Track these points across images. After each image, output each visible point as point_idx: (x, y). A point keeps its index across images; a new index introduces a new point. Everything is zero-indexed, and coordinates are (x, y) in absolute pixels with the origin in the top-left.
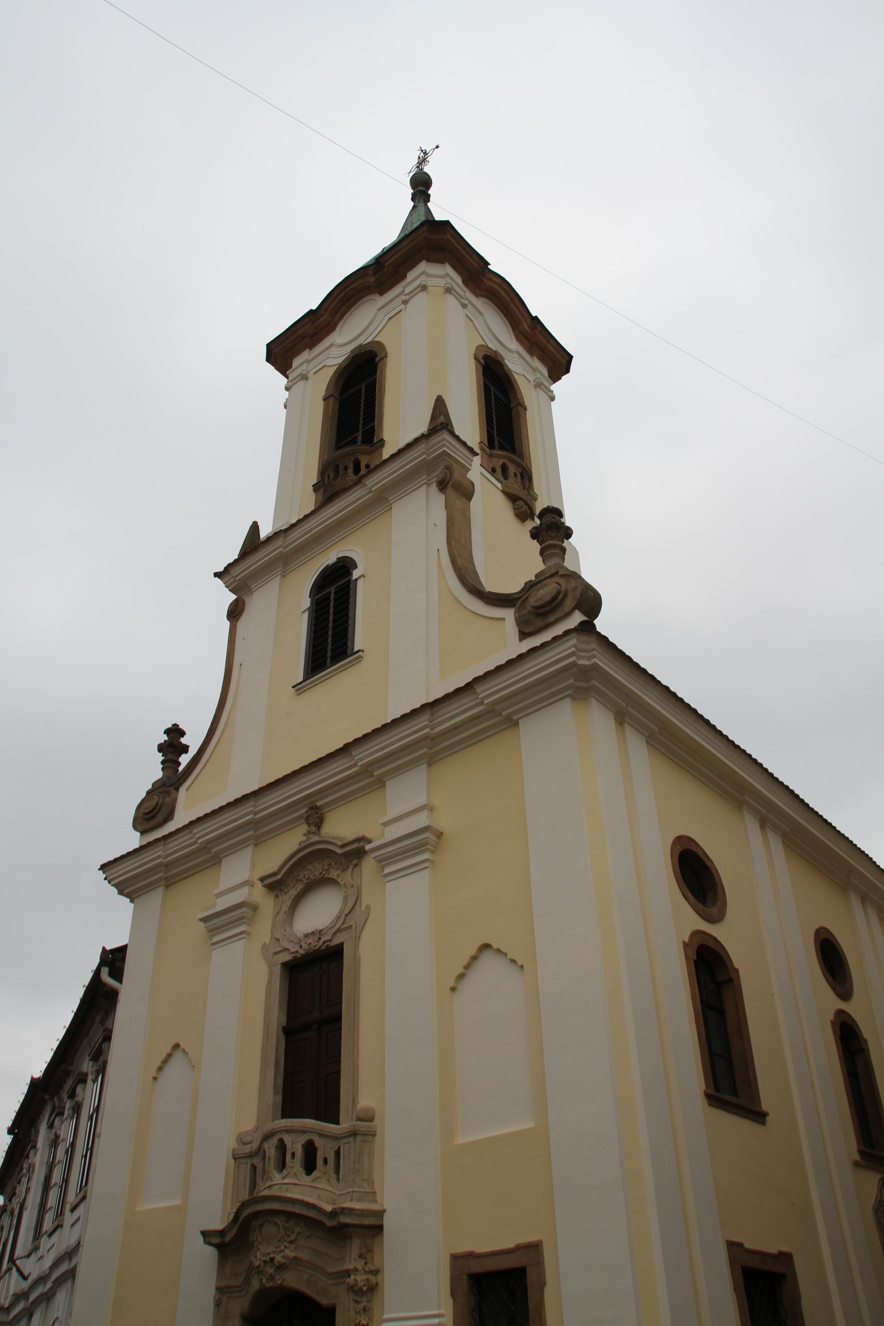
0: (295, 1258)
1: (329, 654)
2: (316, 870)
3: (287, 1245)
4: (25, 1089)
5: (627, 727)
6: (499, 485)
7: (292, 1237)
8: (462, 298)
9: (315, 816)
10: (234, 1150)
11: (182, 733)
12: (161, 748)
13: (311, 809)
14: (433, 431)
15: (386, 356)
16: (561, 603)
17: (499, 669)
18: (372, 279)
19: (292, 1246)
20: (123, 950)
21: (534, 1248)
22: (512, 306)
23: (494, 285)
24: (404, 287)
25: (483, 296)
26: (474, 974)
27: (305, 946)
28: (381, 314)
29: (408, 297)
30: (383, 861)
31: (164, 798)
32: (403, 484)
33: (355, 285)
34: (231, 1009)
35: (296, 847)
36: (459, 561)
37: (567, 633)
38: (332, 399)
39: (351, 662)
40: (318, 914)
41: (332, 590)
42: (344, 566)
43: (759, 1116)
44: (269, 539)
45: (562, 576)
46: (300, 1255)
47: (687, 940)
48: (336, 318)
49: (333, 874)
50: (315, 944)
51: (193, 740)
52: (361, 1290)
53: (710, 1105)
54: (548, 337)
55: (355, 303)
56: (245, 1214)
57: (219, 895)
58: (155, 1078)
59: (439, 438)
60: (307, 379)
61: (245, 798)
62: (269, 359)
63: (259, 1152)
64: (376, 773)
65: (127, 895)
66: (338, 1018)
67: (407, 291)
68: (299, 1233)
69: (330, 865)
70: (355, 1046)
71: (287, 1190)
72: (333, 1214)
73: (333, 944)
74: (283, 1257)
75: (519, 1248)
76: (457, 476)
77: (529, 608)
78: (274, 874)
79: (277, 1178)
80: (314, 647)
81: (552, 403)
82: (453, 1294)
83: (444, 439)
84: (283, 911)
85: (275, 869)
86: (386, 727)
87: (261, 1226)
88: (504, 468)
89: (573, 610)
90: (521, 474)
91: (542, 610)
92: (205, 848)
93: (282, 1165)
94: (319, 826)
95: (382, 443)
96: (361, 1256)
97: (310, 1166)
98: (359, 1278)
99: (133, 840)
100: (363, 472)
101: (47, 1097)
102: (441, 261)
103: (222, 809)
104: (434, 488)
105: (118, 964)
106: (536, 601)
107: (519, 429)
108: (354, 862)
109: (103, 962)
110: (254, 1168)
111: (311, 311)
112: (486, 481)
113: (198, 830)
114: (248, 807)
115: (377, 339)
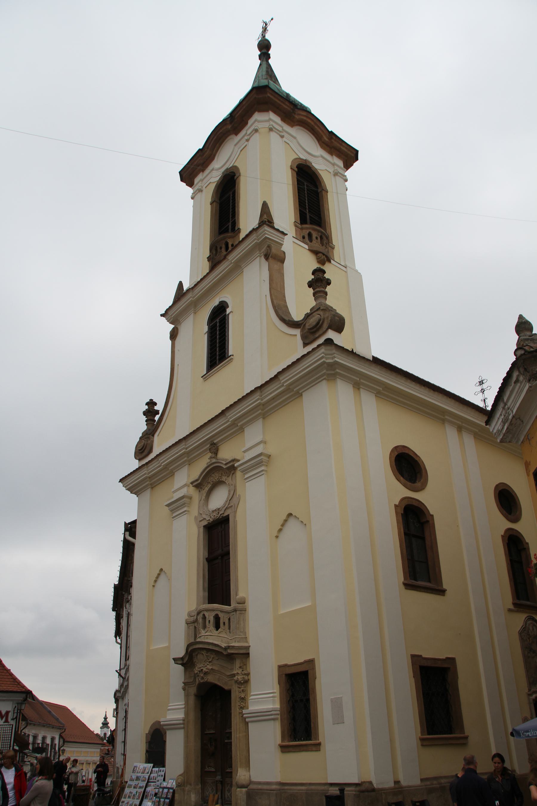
0: (212, 669)
2: (215, 477)
3: (208, 663)
6: (306, 247)
7: (210, 660)
8: (280, 132)
9: (214, 448)
10: (186, 620)
11: (155, 404)
12: (145, 413)
13: (211, 444)
14: (262, 223)
16: (321, 326)
18: (229, 127)
20: (134, 522)
21: (311, 662)
22: (316, 127)
24: (247, 131)
25: (297, 125)
26: (286, 529)
27: (212, 517)
29: (248, 137)
30: (245, 471)
31: (147, 441)
32: (247, 257)
33: (221, 131)
34: (181, 549)
35: (205, 466)
36: (275, 302)
37: (319, 346)
38: (214, 204)
39: (228, 362)
40: (218, 500)
41: (218, 321)
43: (442, 592)
44: (188, 290)
45: (322, 310)
46: (214, 668)
47: (397, 504)
50: (216, 516)
51: (160, 407)
52: (240, 682)
55: (223, 142)
56: (190, 650)
59: (261, 231)
61: (180, 441)
62: (182, 180)
63: (196, 621)
64: (239, 425)
65: (135, 493)
66: (228, 553)
68: (213, 658)
69: (222, 474)
70: (236, 568)
71: (207, 638)
72: (226, 649)
73: (225, 515)
75: (306, 662)
76: (274, 251)
77: (306, 330)
78: (197, 480)
79: (203, 632)
80: (211, 354)
81: (346, 183)
83: (265, 230)
84: (202, 499)
85: (197, 478)
87: (197, 655)
88: (310, 235)
90: (321, 238)
92: (166, 467)
93: (204, 627)
94: (216, 453)
95: (239, 230)
96: (240, 667)
97: (217, 627)
99: (135, 464)
100: (230, 249)
101: (124, 593)
102: (267, 110)
104: (263, 259)
105: (133, 530)
106: (309, 326)
107: (323, 205)
108: (232, 472)
110: (195, 627)
111: (200, 150)
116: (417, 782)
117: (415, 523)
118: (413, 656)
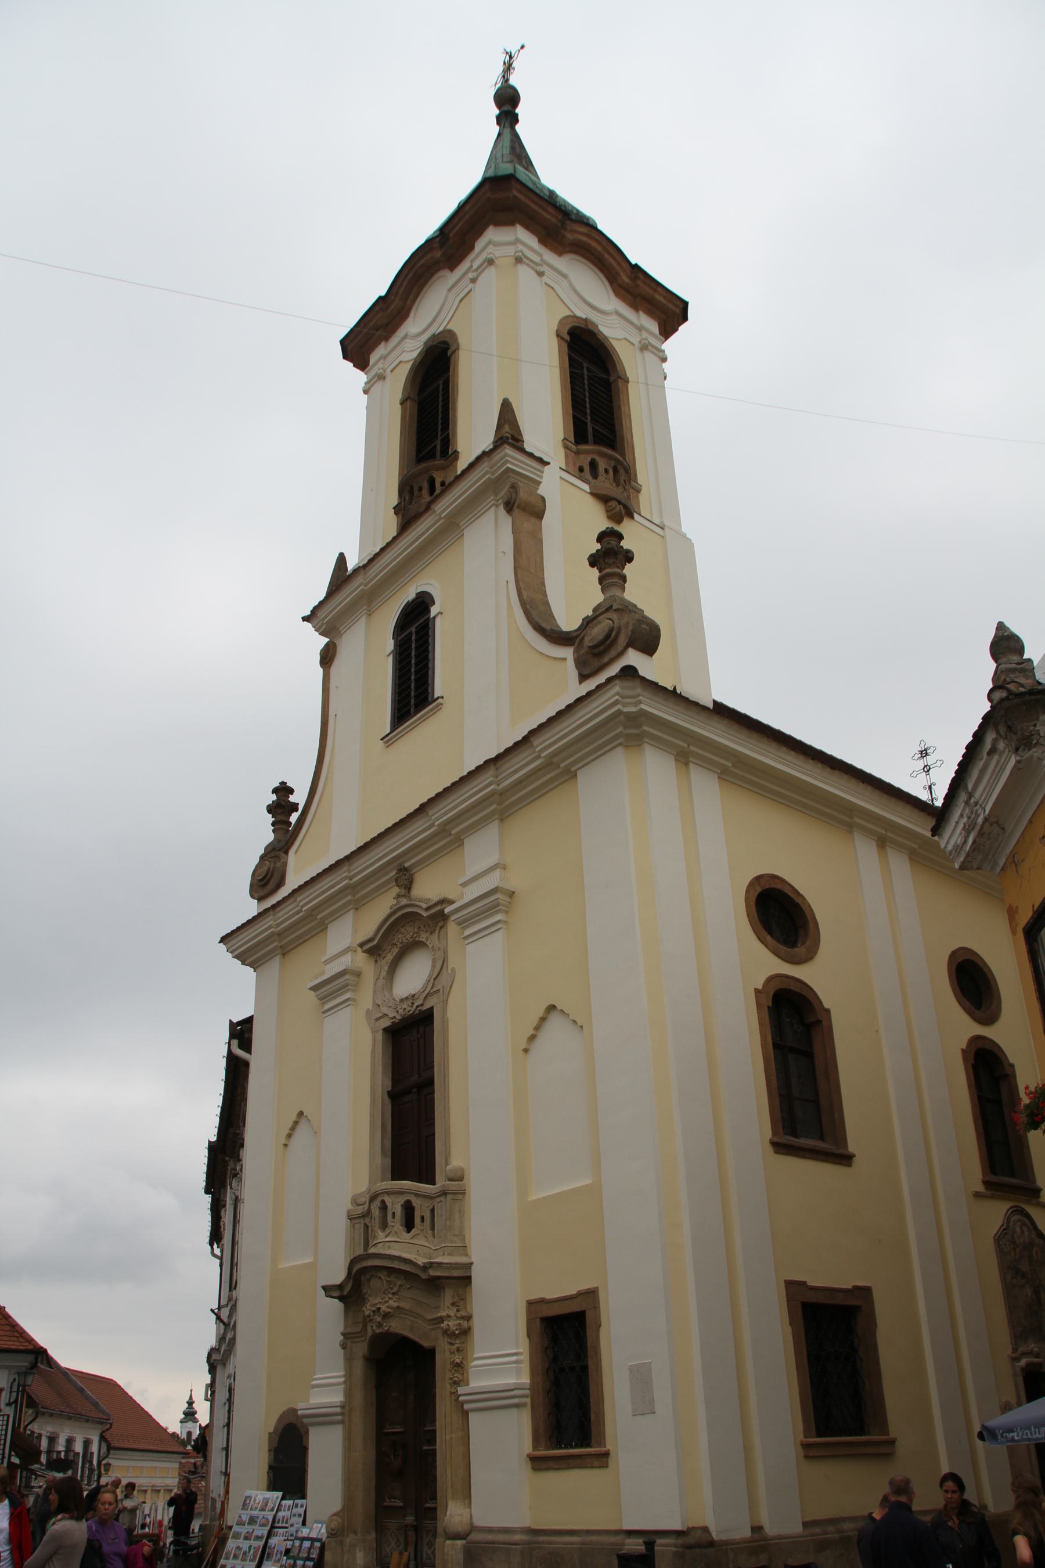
0: (398, 1307)
1: (412, 702)
2: (406, 934)
3: (391, 1296)
5: (692, 766)
7: (395, 1290)
9: (405, 878)
10: (349, 1211)
12: (270, 809)
13: (400, 870)
14: (500, 442)
17: (551, 721)
18: (438, 254)
19: (395, 1298)
20: (249, 1021)
21: (591, 1294)
24: (472, 262)
25: (569, 252)
28: (452, 295)
29: (475, 274)
30: (463, 923)
32: (471, 507)
34: (340, 1073)
35: (388, 911)
37: (609, 680)
38: (409, 402)
40: (413, 978)
41: (413, 629)
43: (845, 1159)
44: (356, 571)
46: (402, 1304)
48: (409, 302)
49: (423, 937)
50: (408, 1009)
51: (299, 797)
53: (776, 1152)
54: (654, 286)
57: (327, 962)
58: (286, 1145)
59: (502, 454)
60: (384, 378)
61: (338, 864)
63: (368, 1213)
65: (250, 965)
66: (431, 1082)
68: (401, 1286)
70: (446, 1109)
71: (389, 1247)
72: (425, 1268)
73: (424, 1008)
75: (581, 1294)
76: (523, 495)
78: (371, 940)
79: (381, 1236)
82: (529, 1336)
83: (506, 455)
85: (370, 935)
86: (463, 780)
87: (369, 1280)
88: (593, 465)
90: (615, 470)
91: (601, 648)
93: (384, 1226)
94: (408, 887)
95: (456, 454)
96: (453, 1304)
97: (409, 1225)
98: (451, 1324)
99: (251, 908)
102: (511, 223)
103: (319, 875)
104: (502, 511)
105: (246, 1035)
107: (619, 407)
108: (440, 924)
110: (366, 1226)
111: (380, 298)
112: (570, 486)
113: (301, 898)
114: (343, 872)
115: (449, 327)
116: (797, 1528)
117: (793, 1025)
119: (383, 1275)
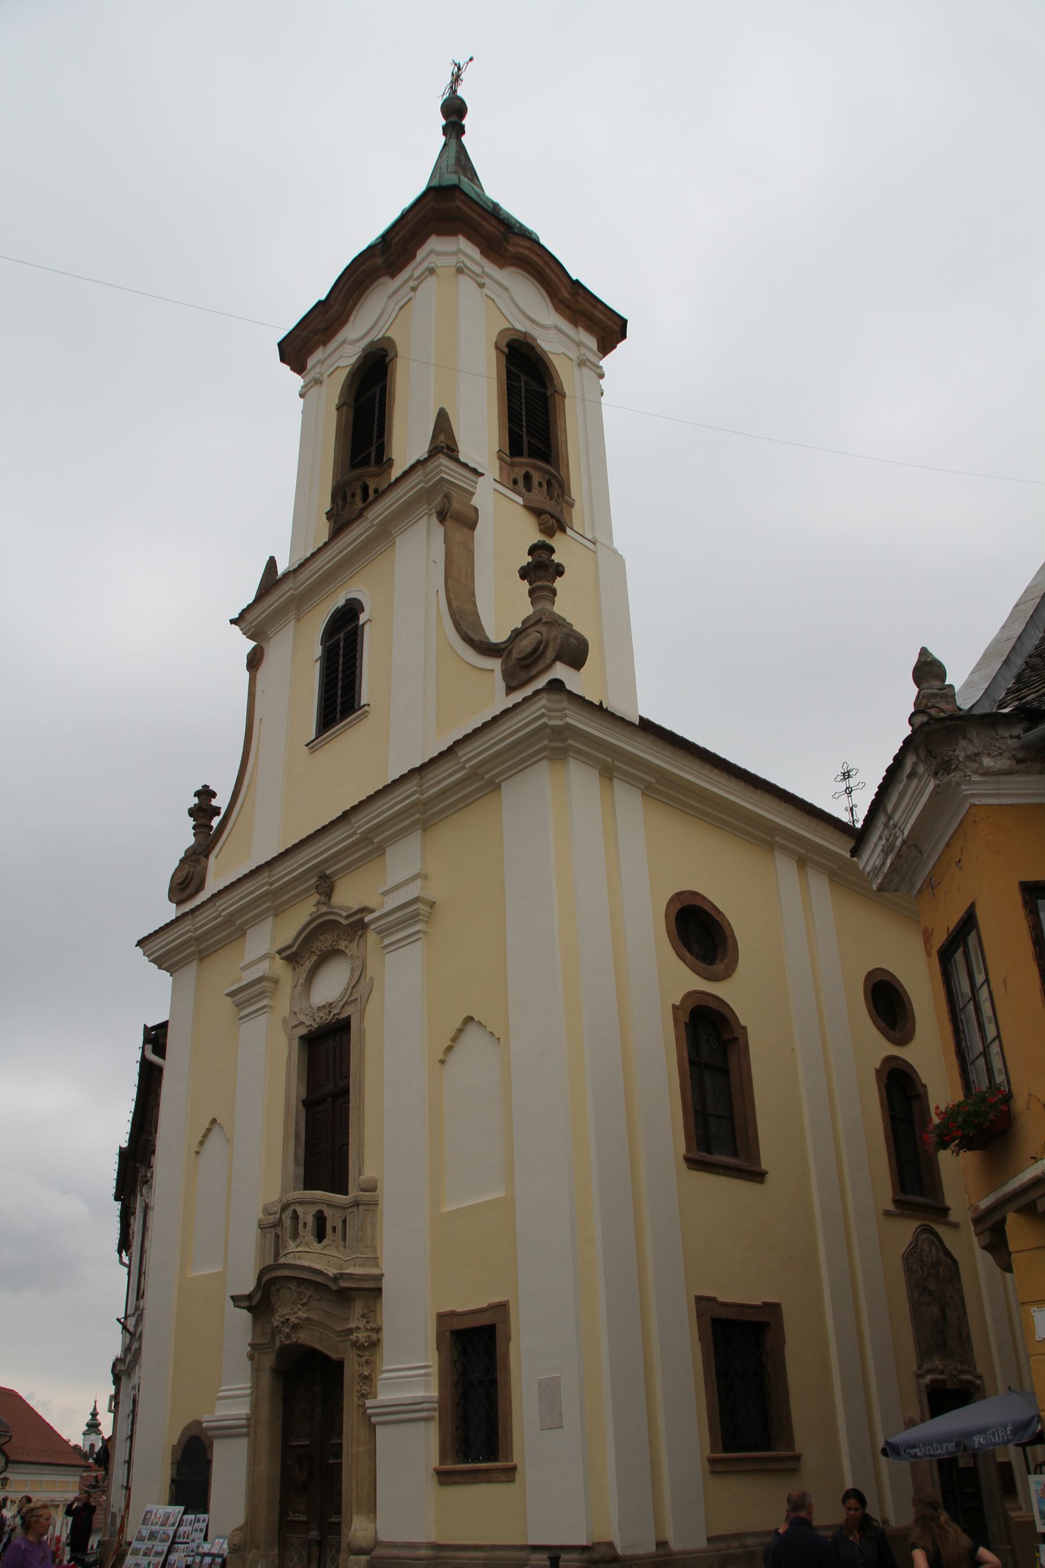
0: (307, 1318)
1: (339, 708)
2: (325, 942)
3: (300, 1307)
4: (117, 1159)
6: (520, 500)
7: (304, 1301)
9: (325, 886)
10: (260, 1221)
11: (214, 795)
12: (192, 812)
13: (321, 878)
14: (435, 451)
15: (396, 356)
16: (543, 654)
18: (380, 261)
20: (163, 1026)
21: (502, 1308)
23: (521, 250)
24: (413, 270)
25: (511, 265)
29: (416, 283)
31: (195, 867)
32: (405, 513)
33: (364, 268)
34: (255, 1083)
35: (307, 918)
36: (455, 604)
37: (536, 693)
40: (330, 986)
41: (342, 636)
42: (352, 609)
43: (758, 1176)
44: (286, 575)
45: (546, 623)
46: (312, 1316)
48: (348, 308)
49: (342, 945)
50: (324, 1017)
51: (221, 801)
55: (367, 289)
56: (264, 1280)
58: (198, 1153)
60: (321, 383)
61: (259, 869)
63: (279, 1223)
65: (167, 969)
66: (346, 1092)
67: (416, 275)
68: (310, 1297)
69: (339, 935)
70: (361, 1119)
71: (300, 1258)
73: (342, 1016)
74: (297, 1318)
76: (456, 505)
78: (290, 947)
79: (292, 1246)
82: (439, 1348)
85: (289, 942)
87: (278, 1291)
88: (527, 478)
89: (553, 662)
90: (549, 484)
92: (229, 920)
93: (295, 1235)
96: (363, 1316)
97: (320, 1235)
99: (170, 912)
101: (138, 1165)
102: (453, 233)
104: (434, 519)
105: (161, 1040)
107: (555, 421)
108: (359, 933)
109: (147, 1040)
110: (277, 1236)
111: (320, 303)
113: (222, 903)
115: (388, 334)
116: (701, 1543)
117: (710, 1041)
118: (699, 1299)
119: (293, 1285)
